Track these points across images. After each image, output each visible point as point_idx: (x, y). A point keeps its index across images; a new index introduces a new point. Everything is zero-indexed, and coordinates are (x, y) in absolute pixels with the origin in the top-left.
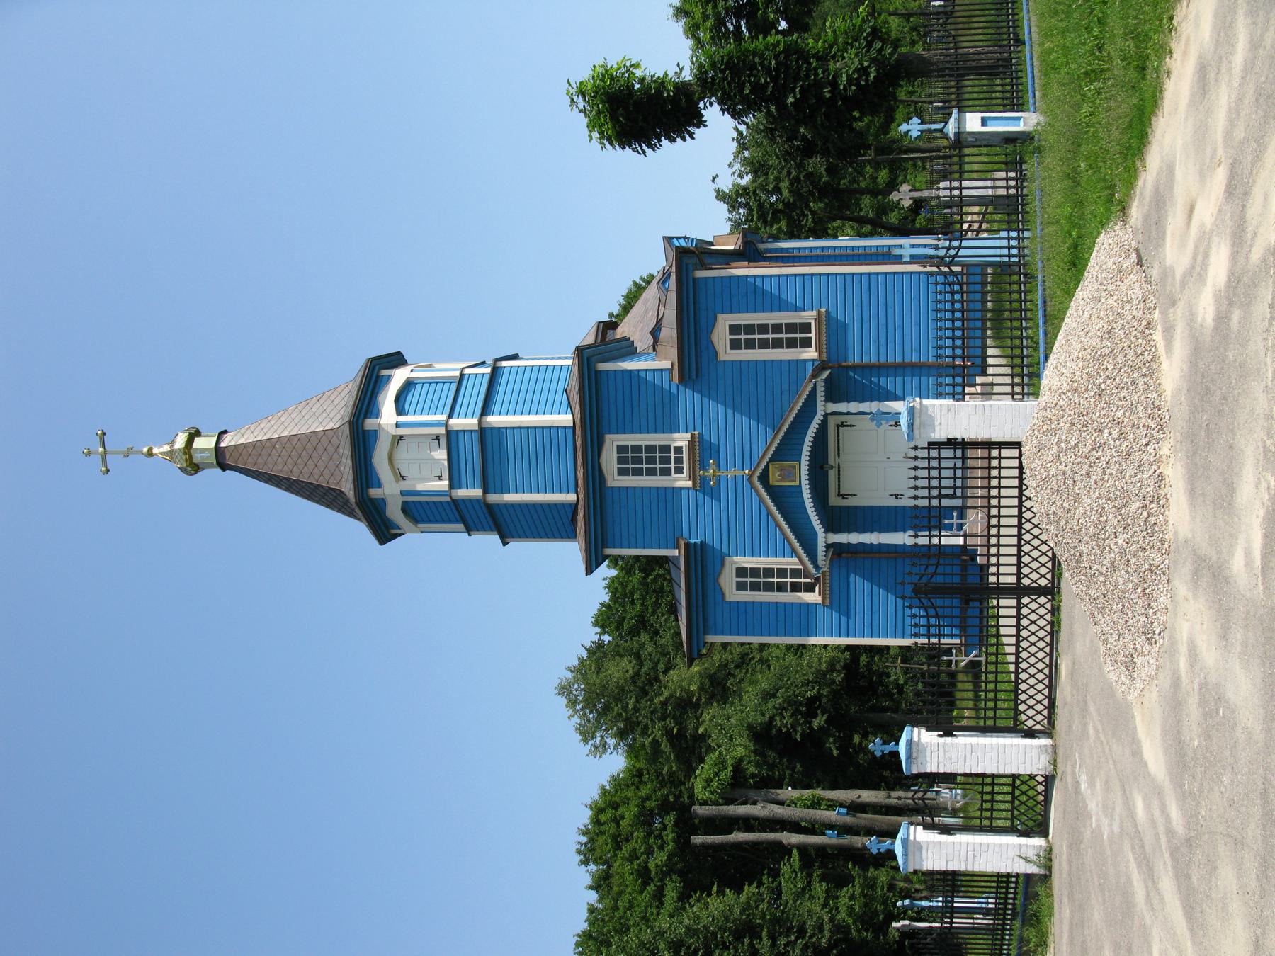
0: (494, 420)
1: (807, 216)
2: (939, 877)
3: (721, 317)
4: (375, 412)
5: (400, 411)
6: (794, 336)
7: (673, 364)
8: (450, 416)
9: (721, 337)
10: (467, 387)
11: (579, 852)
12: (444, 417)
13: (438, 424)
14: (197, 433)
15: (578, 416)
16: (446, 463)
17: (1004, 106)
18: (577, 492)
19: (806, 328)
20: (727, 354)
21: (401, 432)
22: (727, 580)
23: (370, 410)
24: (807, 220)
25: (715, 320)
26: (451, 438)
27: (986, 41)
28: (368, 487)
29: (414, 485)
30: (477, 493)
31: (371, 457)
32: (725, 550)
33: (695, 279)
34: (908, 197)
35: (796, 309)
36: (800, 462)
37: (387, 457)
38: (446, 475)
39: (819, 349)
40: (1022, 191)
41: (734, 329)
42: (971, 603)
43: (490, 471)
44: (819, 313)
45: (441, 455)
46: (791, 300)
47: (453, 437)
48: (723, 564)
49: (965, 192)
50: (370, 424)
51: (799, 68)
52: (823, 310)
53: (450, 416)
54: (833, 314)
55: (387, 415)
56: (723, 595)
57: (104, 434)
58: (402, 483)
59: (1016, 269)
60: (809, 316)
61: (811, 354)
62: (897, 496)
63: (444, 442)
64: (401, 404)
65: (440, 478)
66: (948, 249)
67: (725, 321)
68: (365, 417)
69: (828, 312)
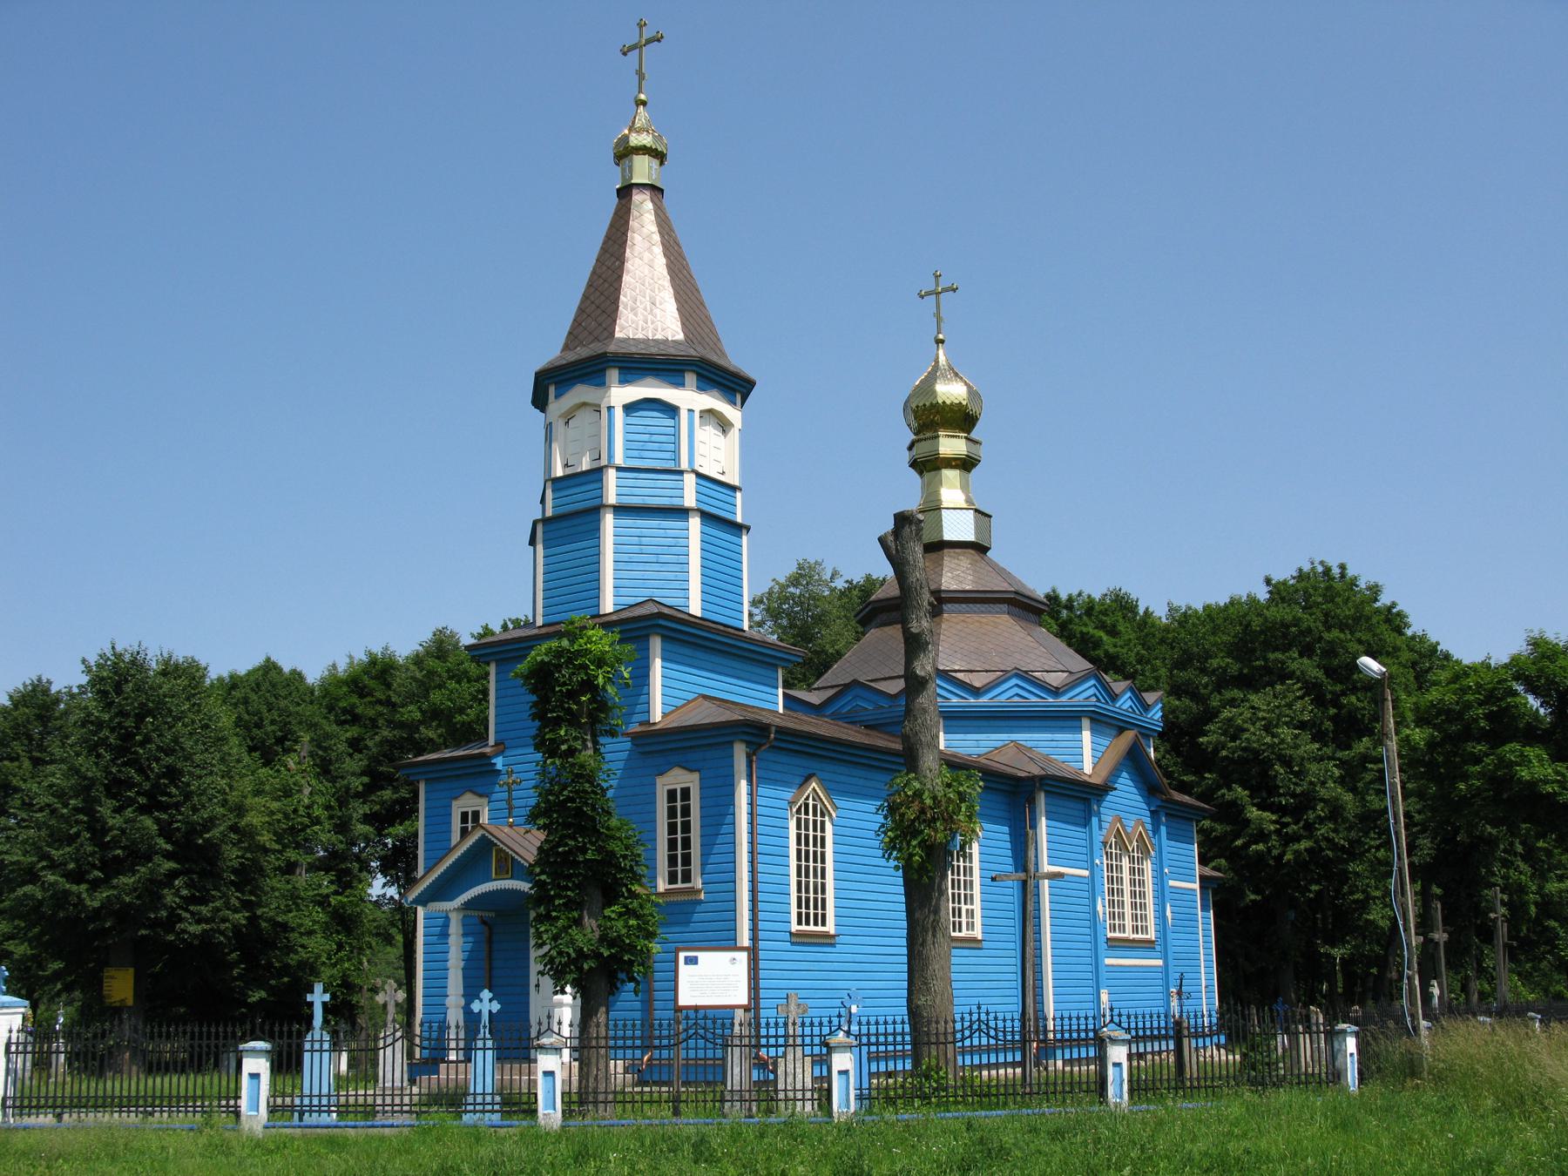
0: (609, 520)
1: (1379, 838)
2: (37, 1046)
3: (696, 776)
4: (629, 377)
5: (630, 408)
6: (680, 865)
7: (655, 724)
8: (619, 469)
9: (677, 778)
10: (667, 481)
11: (39, 680)
12: (619, 460)
13: (611, 456)
14: (659, 156)
15: (614, 618)
16: (579, 470)
17: (861, 1089)
18: (543, 626)
19: (687, 877)
20: (663, 784)
21: (604, 412)
22: (471, 801)
23: (633, 372)
24: (1375, 839)
25: (691, 771)
26: (597, 473)
27: (1213, 1070)
28: (556, 383)
29: (556, 440)
30: (612, 498)
31: (583, 382)
32: (494, 797)
33: (731, 743)
34: (387, 999)
35: (703, 865)
36: (512, 878)
37: (582, 400)
38: (569, 471)
39: (668, 892)
40: (316, 1111)
41: (686, 793)
42: (576, 1064)
43: (576, 521)
44: (699, 891)
45: (586, 465)
46: (712, 859)
47: (594, 477)
48: (481, 796)
49: (480, 1053)
50: (613, 374)
51: (569, 877)
52: (702, 896)
53: (619, 469)
54: (699, 908)
55: (621, 394)
56: (456, 798)
57: (659, 41)
58: (561, 422)
59: (199, 1104)
60: (697, 882)
61: (662, 885)
62: (537, 986)
63: (596, 465)
64: (644, 406)
65: (566, 465)
66: (996, 1029)
67: (692, 781)
68: (620, 368)
69: (700, 902)
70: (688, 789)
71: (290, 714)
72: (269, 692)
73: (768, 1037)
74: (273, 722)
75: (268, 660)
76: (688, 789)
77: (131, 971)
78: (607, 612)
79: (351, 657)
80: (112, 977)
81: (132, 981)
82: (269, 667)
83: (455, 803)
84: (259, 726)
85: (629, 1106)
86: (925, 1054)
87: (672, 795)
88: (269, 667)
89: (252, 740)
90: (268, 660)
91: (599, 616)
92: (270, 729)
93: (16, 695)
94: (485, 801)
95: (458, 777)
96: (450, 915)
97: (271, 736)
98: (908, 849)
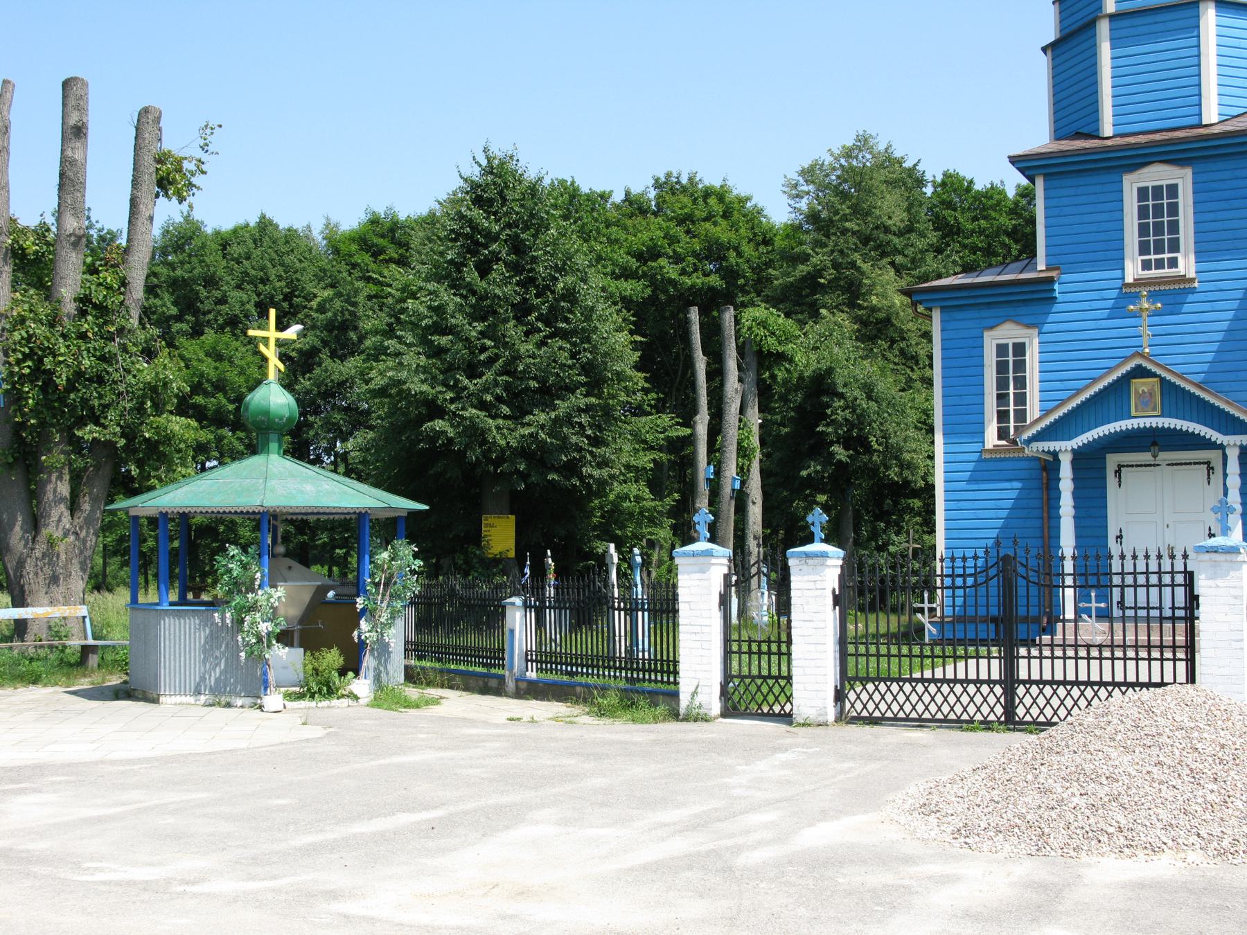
15: (1216, 130)
32: (1046, 328)
48: (1029, 326)
70: (1023, 345)
71: (297, 271)
72: (270, 247)
73: (964, 587)
74: (280, 278)
75: (263, 217)
76: (1023, 345)
77: (513, 517)
78: (1213, 121)
79: (328, 219)
80: (492, 526)
81: (513, 534)
82: (265, 224)
83: (987, 334)
84: (264, 281)
85: (917, 660)
86: (993, 601)
87: (1002, 349)
88: (265, 224)
89: (258, 295)
90: (263, 217)
91: (1201, 126)
92: (278, 284)
93: (512, 166)
94: (1035, 332)
95: (989, 305)
96: (1061, 457)
97: (279, 292)
98: (572, 434)
